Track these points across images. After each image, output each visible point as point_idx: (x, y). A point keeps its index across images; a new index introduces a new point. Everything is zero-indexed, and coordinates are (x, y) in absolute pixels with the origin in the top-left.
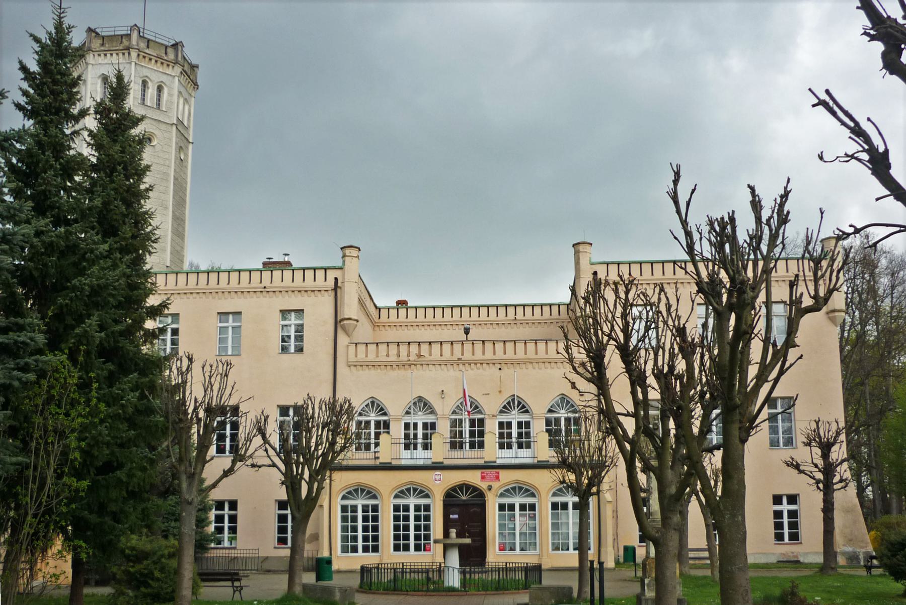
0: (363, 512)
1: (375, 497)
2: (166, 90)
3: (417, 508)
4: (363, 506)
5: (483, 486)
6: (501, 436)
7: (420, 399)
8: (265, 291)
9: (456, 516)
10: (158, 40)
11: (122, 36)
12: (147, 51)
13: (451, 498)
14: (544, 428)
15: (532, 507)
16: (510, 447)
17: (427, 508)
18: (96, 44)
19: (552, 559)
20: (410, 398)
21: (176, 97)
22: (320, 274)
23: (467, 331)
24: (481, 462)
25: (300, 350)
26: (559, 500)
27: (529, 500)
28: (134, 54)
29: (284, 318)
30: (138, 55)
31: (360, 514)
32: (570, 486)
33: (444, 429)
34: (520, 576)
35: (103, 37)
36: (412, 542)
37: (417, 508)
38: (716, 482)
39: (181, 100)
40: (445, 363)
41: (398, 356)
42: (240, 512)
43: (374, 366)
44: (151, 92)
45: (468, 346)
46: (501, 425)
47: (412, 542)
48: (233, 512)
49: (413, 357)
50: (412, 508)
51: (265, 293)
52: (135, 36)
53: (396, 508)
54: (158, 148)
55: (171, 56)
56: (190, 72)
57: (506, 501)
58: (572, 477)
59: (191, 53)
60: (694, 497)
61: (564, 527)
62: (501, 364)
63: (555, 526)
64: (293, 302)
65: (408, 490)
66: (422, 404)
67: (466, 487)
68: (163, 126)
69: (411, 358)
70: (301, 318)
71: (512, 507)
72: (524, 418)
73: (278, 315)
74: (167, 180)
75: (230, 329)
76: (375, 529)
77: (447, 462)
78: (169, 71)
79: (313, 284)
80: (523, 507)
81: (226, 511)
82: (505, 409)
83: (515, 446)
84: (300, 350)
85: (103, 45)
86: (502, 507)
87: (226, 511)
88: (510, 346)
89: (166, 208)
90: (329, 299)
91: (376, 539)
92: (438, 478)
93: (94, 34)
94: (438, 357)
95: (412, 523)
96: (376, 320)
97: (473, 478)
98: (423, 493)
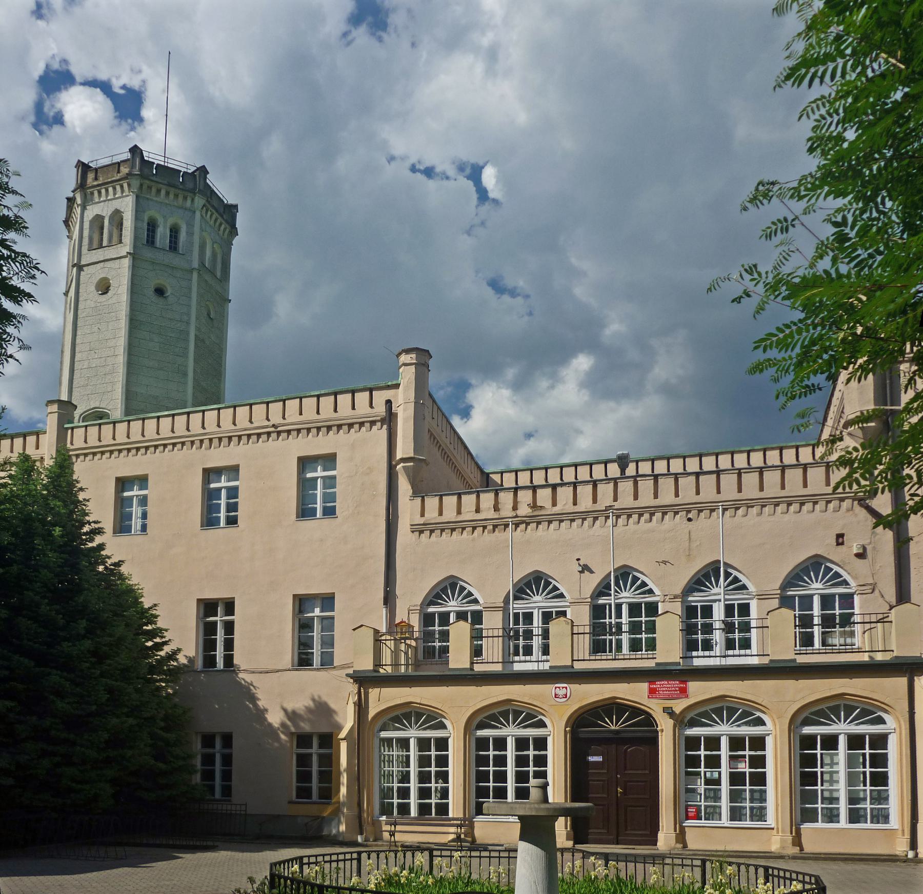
8: (277, 432)
9: (599, 759)
11: (119, 164)
13: (583, 725)
30: (141, 185)
35: (96, 170)
40: (584, 516)
41: (496, 508)
43: (452, 528)
44: (162, 233)
45: (626, 487)
48: (227, 751)
54: (171, 299)
64: (128, 466)
67: (612, 707)
74: (187, 340)
79: (352, 413)
81: (315, 749)
82: (700, 582)
84: (329, 512)
85: (96, 179)
87: (315, 749)
89: (185, 374)
90: (381, 434)
92: (563, 692)
94: (570, 508)
97: (635, 693)
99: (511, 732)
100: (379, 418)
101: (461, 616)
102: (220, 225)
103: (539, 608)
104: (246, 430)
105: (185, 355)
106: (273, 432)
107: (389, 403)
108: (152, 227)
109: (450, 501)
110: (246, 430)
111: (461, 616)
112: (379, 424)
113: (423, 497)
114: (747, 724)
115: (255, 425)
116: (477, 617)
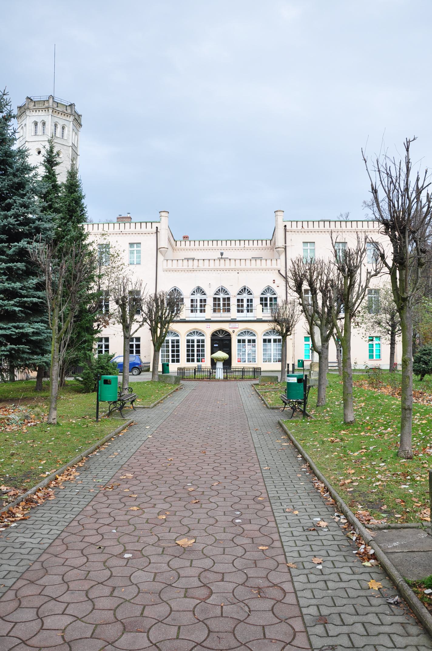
0: (197, 342)
1: (177, 336)
2: (66, 129)
3: (198, 341)
5: (230, 331)
6: (238, 306)
7: (198, 288)
9: (217, 345)
10: (62, 103)
12: (57, 109)
13: (214, 336)
14: (260, 302)
15: (254, 341)
16: (242, 311)
17: (203, 341)
18: (31, 105)
19: (265, 367)
20: (193, 287)
21: (71, 132)
22: (149, 225)
23: (222, 254)
24: (229, 319)
26: (267, 337)
27: (252, 338)
28: (51, 110)
29: (130, 247)
32: (278, 331)
33: (210, 303)
34: (251, 374)
36: (196, 358)
37: (198, 341)
38: (342, 330)
39: (74, 133)
40: (211, 270)
42: (110, 343)
44: (59, 129)
46: (238, 300)
47: (196, 358)
49: (195, 267)
50: (196, 341)
52: (51, 100)
53: (188, 341)
55: (69, 111)
56: (77, 120)
57: (241, 338)
58: (279, 327)
59: (78, 109)
60: (332, 337)
61: (269, 351)
62: (238, 270)
63: (265, 350)
65: (194, 332)
66: (199, 290)
67: (221, 331)
69: (194, 267)
70: (140, 247)
71: (244, 341)
72: (250, 297)
73: (128, 245)
75: (135, 251)
77: (213, 319)
78: (68, 119)
80: (249, 341)
83: (245, 311)
85: (35, 106)
86: (239, 341)
88: (243, 261)
91: (178, 356)
93: (30, 100)
94: (249, 267)
95: (196, 348)
96: (175, 246)
97: (226, 327)
98: (201, 334)
108: (56, 126)
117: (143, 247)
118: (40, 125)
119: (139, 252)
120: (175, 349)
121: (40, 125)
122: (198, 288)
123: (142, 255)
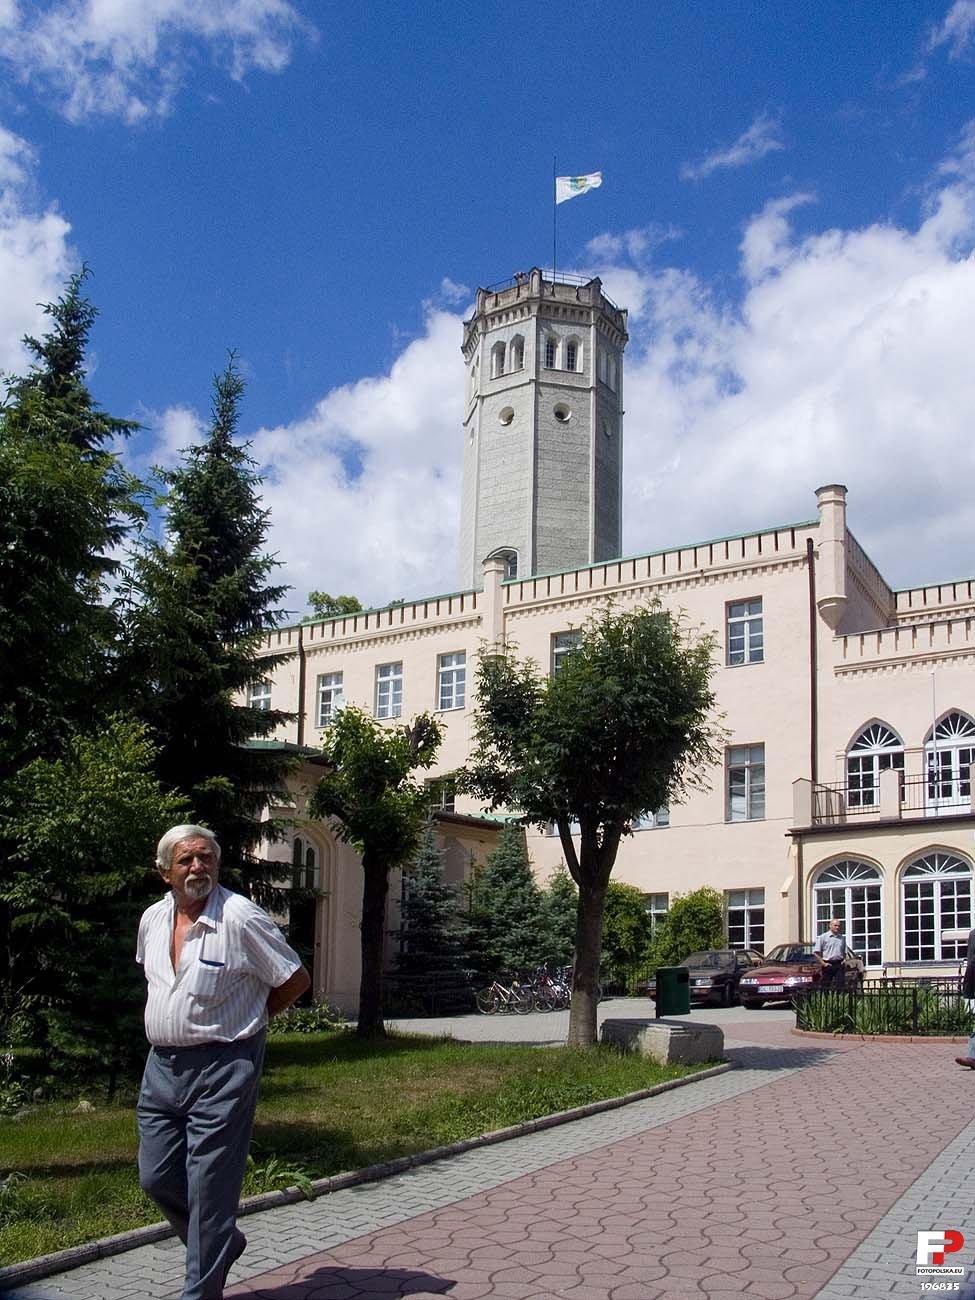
3: (947, 888)
4: (854, 890)
8: (703, 577)
10: (566, 282)
17: (875, 893)
25: (757, 657)
31: (848, 904)
37: (947, 888)
51: (702, 581)
64: (385, 653)
68: (577, 394)
74: (587, 464)
75: (747, 625)
76: (911, 923)
85: (496, 305)
99: (848, 883)
100: (801, 558)
101: (885, 762)
102: (613, 332)
103: (957, 747)
104: (676, 577)
105: (585, 481)
106: (701, 578)
107: (810, 541)
109: (871, 639)
110: (676, 577)
111: (885, 762)
112: (801, 564)
113: (845, 637)
114: (956, 869)
115: (684, 571)
116: (899, 760)
117: (767, 612)
118: (510, 354)
119: (398, 684)
120: (956, 913)
121: (510, 354)
122: (727, 603)
123: (767, 633)
